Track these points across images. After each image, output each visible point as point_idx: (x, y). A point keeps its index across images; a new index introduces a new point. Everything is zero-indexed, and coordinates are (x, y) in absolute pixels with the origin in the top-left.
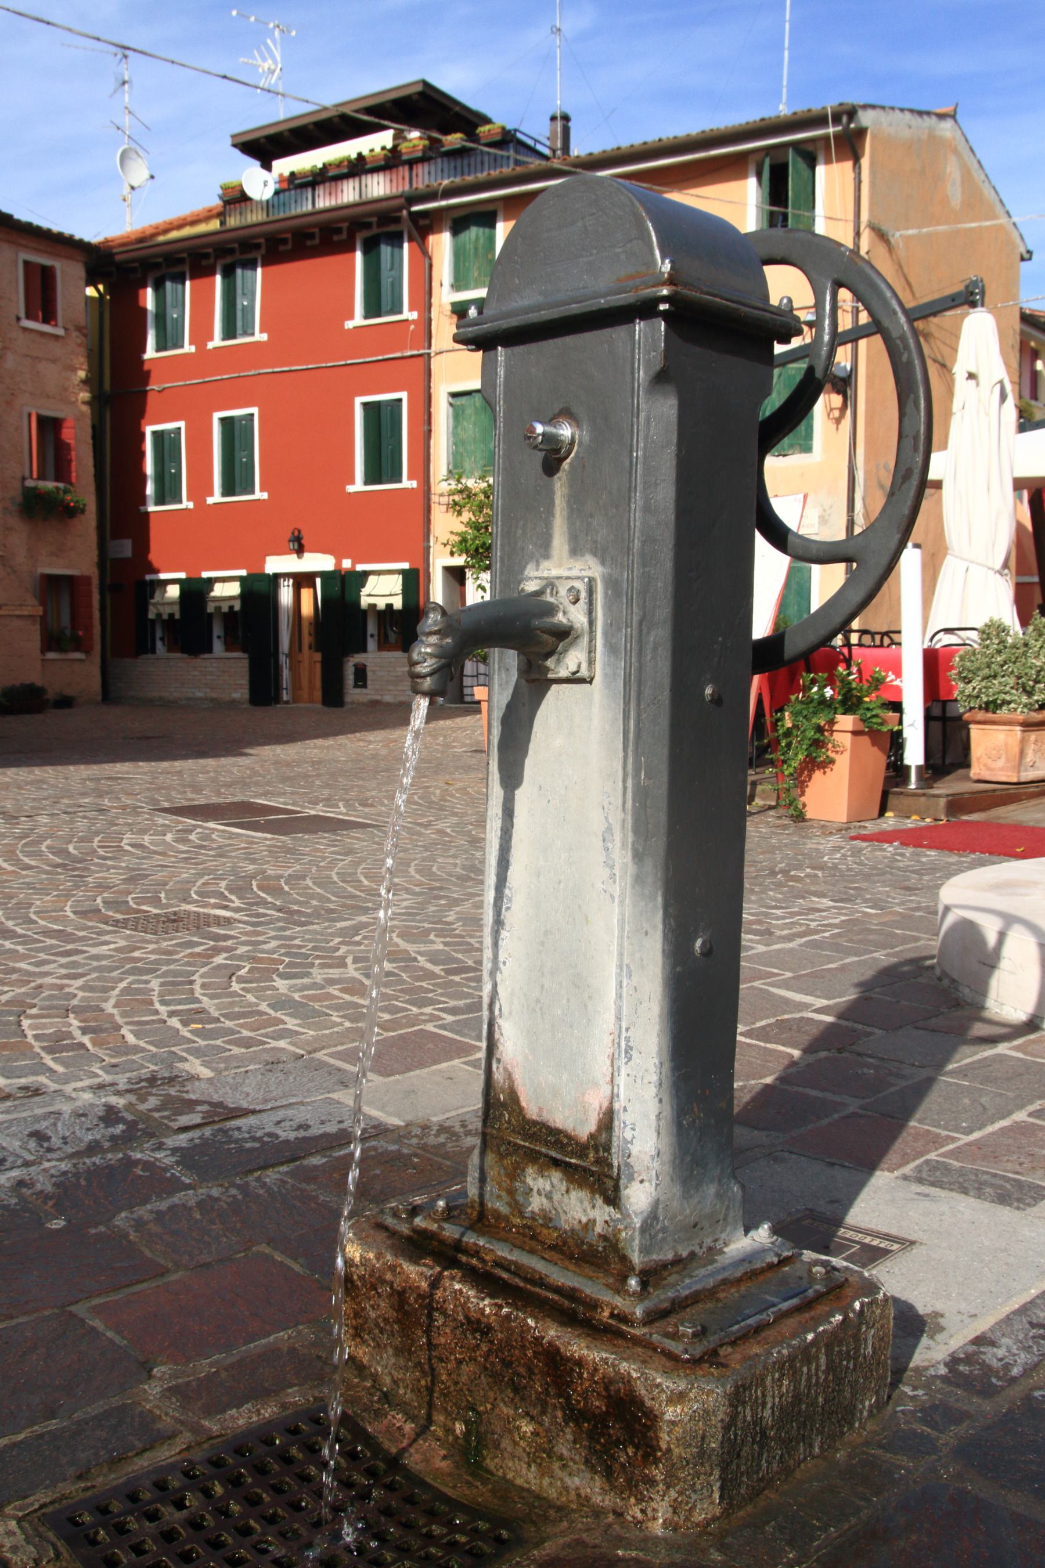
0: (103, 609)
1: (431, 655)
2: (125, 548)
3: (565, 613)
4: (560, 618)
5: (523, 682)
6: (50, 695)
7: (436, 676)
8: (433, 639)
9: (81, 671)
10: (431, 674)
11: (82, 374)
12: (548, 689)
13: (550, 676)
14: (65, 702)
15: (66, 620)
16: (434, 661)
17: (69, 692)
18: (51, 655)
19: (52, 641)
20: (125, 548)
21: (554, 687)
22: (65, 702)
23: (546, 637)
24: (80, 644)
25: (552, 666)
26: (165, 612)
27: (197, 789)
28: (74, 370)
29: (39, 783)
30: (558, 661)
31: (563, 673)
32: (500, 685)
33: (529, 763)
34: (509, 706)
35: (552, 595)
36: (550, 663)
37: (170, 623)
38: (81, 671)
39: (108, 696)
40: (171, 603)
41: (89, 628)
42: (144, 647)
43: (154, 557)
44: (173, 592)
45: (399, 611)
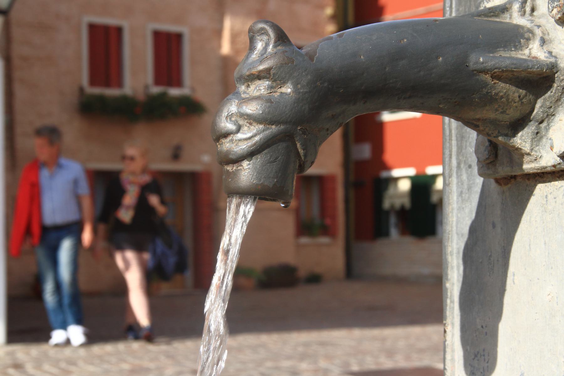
0: (347, 201)
1: (252, 119)
2: (365, 151)
3: (543, 42)
4: (535, 51)
5: (493, 184)
6: (302, 273)
7: (258, 160)
8: (260, 88)
9: (328, 254)
10: (250, 155)
11: (329, 11)
12: (530, 193)
13: (528, 166)
14: (314, 279)
15: (315, 210)
16: (256, 128)
17: (318, 270)
18: (304, 240)
19: (304, 228)
20: (365, 151)
21: (541, 189)
22: (314, 279)
23: (502, 87)
24: (326, 230)
25: (526, 148)
26: (398, 203)
27: (390, 354)
28: (322, 7)
29: (254, 348)
30: (538, 135)
31: (548, 159)
32: (461, 194)
33: (504, 329)
34: (473, 230)
35: (523, 13)
36: (522, 140)
37: (402, 213)
38: (328, 254)
39: (350, 272)
40: (402, 195)
41: (334, 217)
42: (379, 231)
43: (389, 156)
44: (405, 186)
45: (378, 114)
